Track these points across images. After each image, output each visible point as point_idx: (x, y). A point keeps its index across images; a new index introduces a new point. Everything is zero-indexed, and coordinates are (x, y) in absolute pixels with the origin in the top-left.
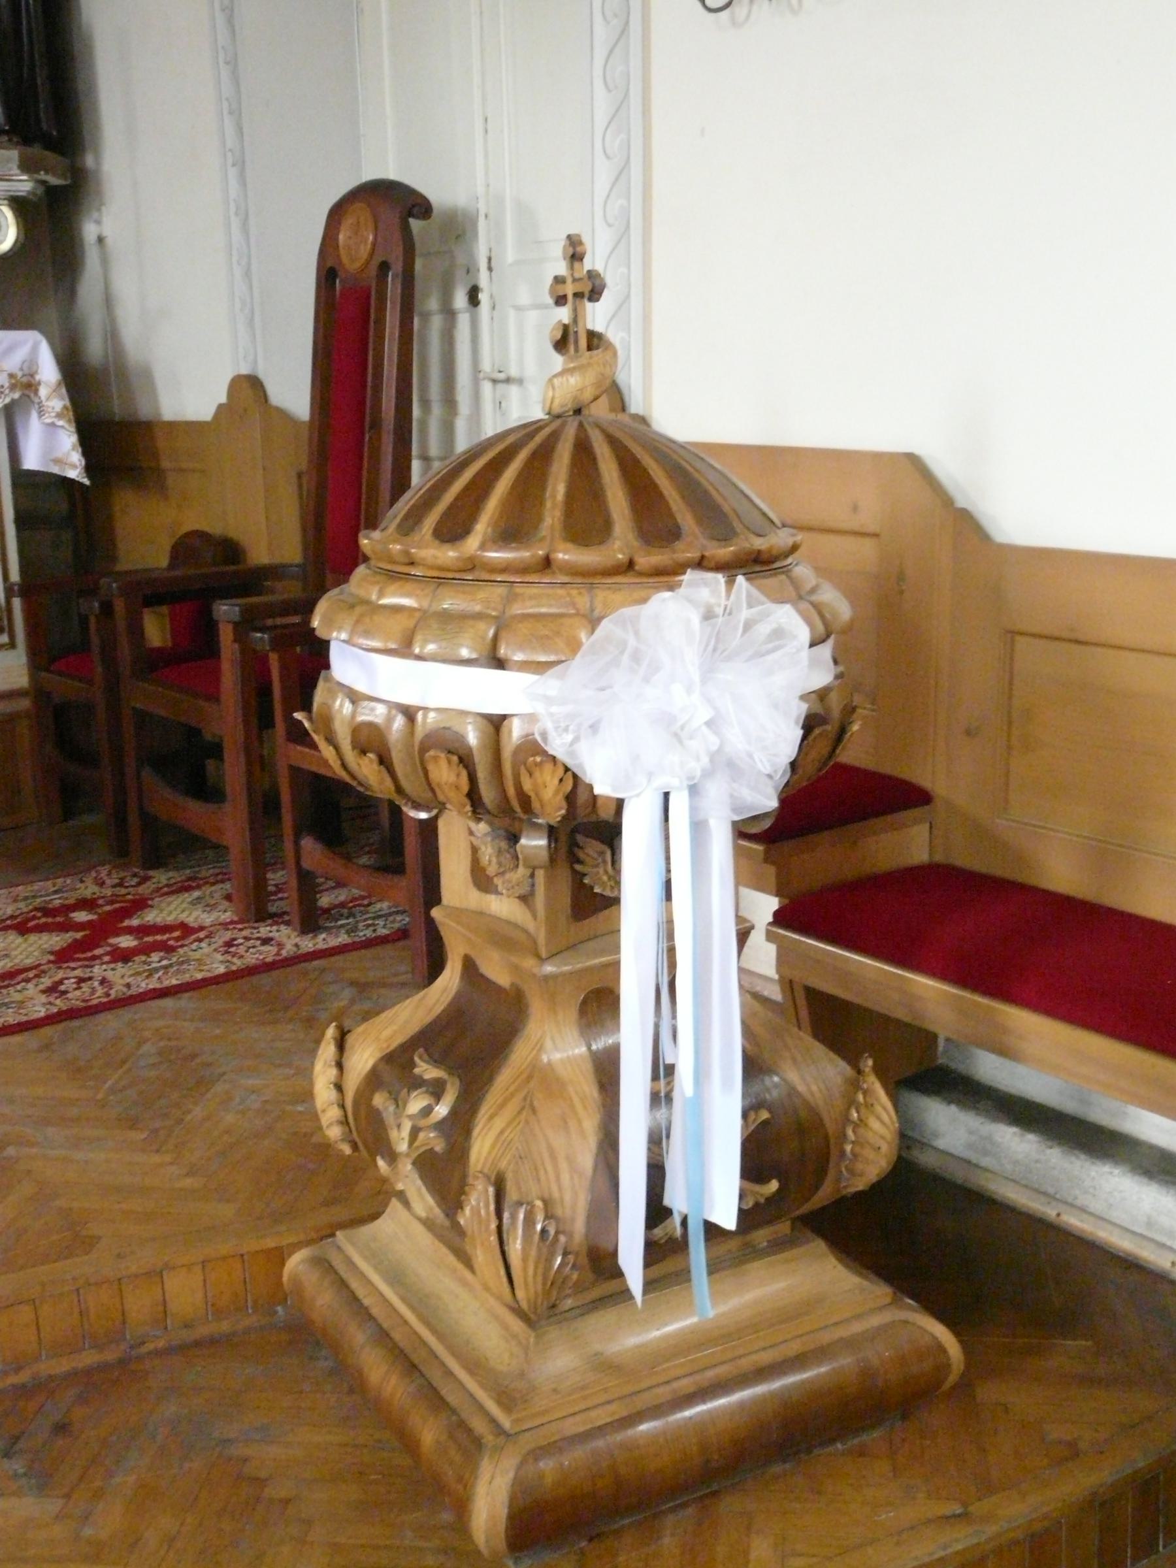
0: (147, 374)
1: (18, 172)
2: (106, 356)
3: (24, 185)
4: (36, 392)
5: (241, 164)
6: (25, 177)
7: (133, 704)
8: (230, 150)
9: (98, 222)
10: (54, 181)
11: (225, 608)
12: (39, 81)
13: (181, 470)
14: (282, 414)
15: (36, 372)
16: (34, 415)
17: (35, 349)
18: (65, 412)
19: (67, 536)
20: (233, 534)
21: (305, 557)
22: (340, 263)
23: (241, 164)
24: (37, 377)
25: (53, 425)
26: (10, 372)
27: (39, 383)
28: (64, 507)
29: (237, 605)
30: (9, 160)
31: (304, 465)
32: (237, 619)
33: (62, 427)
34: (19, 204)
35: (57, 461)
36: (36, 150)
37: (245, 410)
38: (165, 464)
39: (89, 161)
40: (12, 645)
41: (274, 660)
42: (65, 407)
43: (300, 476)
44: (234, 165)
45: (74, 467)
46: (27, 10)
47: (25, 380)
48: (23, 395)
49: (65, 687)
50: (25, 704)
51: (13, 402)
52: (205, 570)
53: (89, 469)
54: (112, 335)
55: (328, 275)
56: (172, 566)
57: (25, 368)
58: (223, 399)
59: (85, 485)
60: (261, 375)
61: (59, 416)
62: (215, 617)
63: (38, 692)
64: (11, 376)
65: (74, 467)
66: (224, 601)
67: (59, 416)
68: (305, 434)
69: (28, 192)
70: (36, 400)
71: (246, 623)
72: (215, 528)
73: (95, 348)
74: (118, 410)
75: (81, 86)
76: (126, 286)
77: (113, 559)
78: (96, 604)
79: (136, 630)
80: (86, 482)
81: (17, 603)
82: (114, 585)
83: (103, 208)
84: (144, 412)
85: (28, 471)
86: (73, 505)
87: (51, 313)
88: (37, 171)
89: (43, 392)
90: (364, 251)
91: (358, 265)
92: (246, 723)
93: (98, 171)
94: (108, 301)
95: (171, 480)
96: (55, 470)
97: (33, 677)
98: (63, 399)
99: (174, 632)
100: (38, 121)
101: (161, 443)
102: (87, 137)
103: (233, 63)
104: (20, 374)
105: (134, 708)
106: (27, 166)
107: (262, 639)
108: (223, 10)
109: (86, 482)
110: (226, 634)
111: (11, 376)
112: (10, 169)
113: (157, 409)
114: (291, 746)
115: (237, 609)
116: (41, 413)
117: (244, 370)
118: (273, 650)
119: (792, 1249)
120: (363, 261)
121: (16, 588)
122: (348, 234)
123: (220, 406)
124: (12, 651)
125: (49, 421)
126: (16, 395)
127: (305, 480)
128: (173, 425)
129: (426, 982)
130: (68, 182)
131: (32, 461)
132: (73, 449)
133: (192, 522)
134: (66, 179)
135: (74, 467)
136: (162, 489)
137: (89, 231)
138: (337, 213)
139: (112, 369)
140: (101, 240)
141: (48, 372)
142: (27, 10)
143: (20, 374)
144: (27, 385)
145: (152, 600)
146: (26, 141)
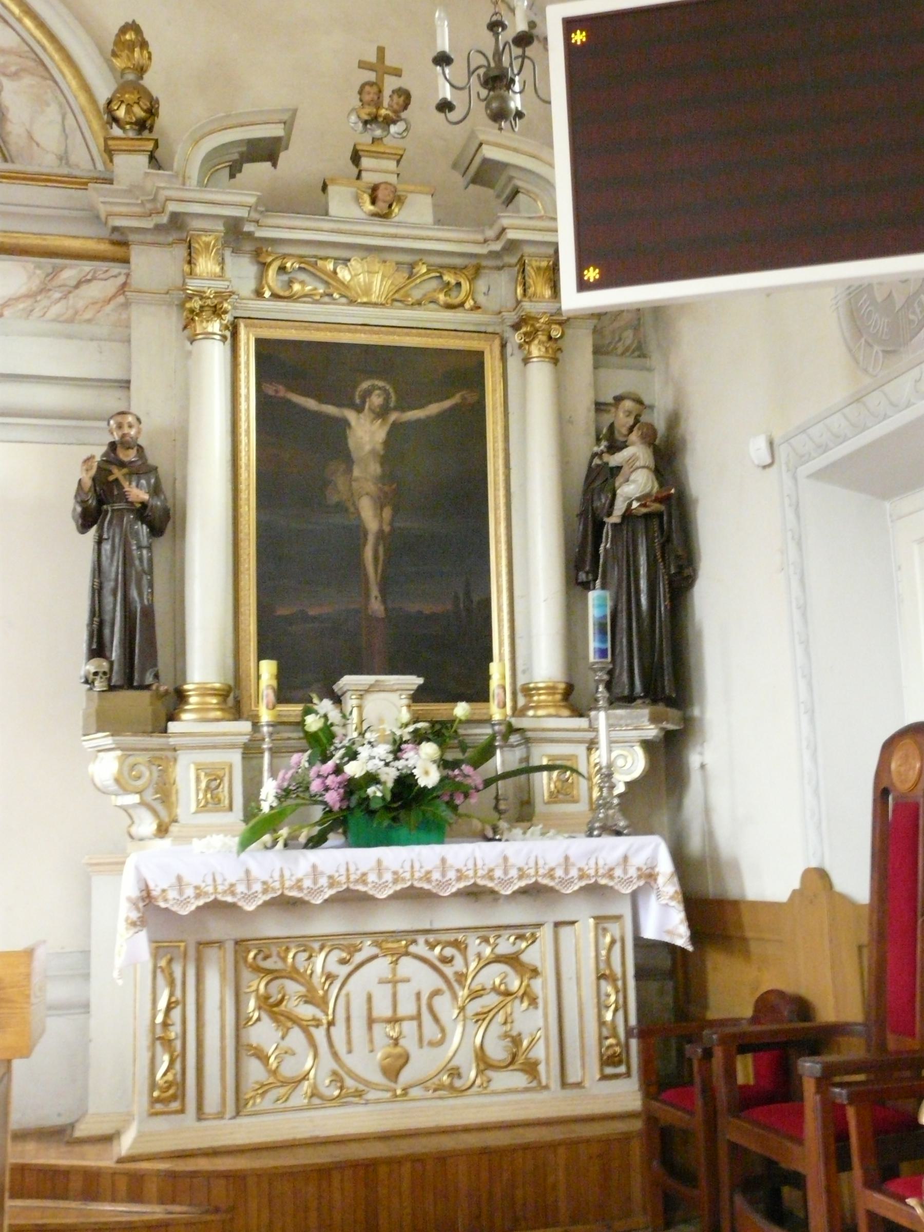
0: (735, 866)
1: (648, 723)
2: (704, 846)
3: (652, 732)
4: (655, 880)
5: (811, 712)
6: (652, 726)
7: (728, 1137)
8: (803, 703)
9: (701, 754)
10: (671, 727)
11: (808, 1064)
12: (665, 663)
13: (763, 939)
14: (845, 899)
15: (656, 866)
16: (653, 897)
17: (656, 850)
18: (676, 896)
19: (669, 985)
20: (803, 992)
21: (867, 1014)
22: (892, 784)
23: (811, 712)
24: (657, 870)
25: (667, 905)
26: (637, 866)
27: (658, 874)
28: (668, 963)
29: (817, 1063)
30: (643, 716)
31: (865, 938)
32: (818, 1075)
33: (673, 907)
34: (647, 745)
35: (669, 932)
36: (661, 708)
37: (815, 896)
38: (749, 934)
39: (696, 712)
40: (628, 1074)
41: (851, 1112)
42: (676, 892)
43: (860, 948)
44: (806, 713)
45: (681, 937)
46: (660, 617)
47: (648, 871)
48: (646, 883)
49: (671, 1115)
50: (637, 1125)
51: (639, 888)
52: (786, 1026)
53: (695, 937)
54: (709, 835)
55: (882, 794)
56: (755, 1020)
57: (649, 862)
58: (796, 885)
59: (689, 951)
60: (828, 868)
61: (672, 898)
62: (800, 1072)
63: (649, 1117)
64: (639, 869)
65: (681, 937)
66: (807, 1058)
67: (672, 898)
68: (866, 913)
69: (654, 736)
70: (655, 887)
71: (825, 1080)
72: (789, 987)
73: (695, 844)
74: (711, 890)
75: (693, 661)
76: (720, 798)
77: (705, 1007)
78: (700, 1050)
79: (730, 1073)
80: (690, 948)
81: (634, 1043)
82: (715, 1037)
83: (705, 744)
84: (733, 893)
85: (648, 940)
86: (674, 960)
87: (663, 818)
88: (662, 722)
89: (661, 880)
90: (913, 776)
91: (909, 785)
92: (826, 1164)
93: (701, 719)
94: (707, 811)
95: (754, 946)
96: (667, 939)
97: (645, 1105)
98: (674, 886)
99: (757, 1074)
100: (663, 688)
101: (747, 919)
102: (695, 694)
103: (806, 644)
104: (644, 868)
105: (729, 1141)
106: (654, 719)
107: (840, 1094)
108: (799, 608)
109: (690, 948)
110: (809, 1088)
111: (639, 869)
112: (643, 722)
113: (742, 887)
114: (868, 1192)
115: (818, 1066)
116: (658, 896)
117: (814, 864)
118: (850, 1103)
119: (529, 1143)
120: (910, 784)
121: (635, 1031)
122: (899, 763)
123: (794, 892)
124: (628, 1079)
125: (664, 902)
126: (641, 883)
127: (865, 951)
128: (755, 905)
129: (150, 728)
130: (682, 727)
131: (650, 932)
132: (681, 922)
133: (771, 981)
134: (679, 725)
135: (681, 936)
136: (746, 954)
137: (694, 759)
138: (889, 746)
139: (708, 860)
140: (703, 766)
141: (665, 866)
142: (660, 617)
143: (644, 868)
144: (650, 876)
145: (743, 1049)
146: (655, 701)
